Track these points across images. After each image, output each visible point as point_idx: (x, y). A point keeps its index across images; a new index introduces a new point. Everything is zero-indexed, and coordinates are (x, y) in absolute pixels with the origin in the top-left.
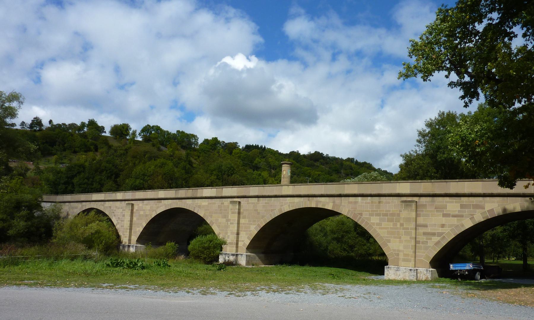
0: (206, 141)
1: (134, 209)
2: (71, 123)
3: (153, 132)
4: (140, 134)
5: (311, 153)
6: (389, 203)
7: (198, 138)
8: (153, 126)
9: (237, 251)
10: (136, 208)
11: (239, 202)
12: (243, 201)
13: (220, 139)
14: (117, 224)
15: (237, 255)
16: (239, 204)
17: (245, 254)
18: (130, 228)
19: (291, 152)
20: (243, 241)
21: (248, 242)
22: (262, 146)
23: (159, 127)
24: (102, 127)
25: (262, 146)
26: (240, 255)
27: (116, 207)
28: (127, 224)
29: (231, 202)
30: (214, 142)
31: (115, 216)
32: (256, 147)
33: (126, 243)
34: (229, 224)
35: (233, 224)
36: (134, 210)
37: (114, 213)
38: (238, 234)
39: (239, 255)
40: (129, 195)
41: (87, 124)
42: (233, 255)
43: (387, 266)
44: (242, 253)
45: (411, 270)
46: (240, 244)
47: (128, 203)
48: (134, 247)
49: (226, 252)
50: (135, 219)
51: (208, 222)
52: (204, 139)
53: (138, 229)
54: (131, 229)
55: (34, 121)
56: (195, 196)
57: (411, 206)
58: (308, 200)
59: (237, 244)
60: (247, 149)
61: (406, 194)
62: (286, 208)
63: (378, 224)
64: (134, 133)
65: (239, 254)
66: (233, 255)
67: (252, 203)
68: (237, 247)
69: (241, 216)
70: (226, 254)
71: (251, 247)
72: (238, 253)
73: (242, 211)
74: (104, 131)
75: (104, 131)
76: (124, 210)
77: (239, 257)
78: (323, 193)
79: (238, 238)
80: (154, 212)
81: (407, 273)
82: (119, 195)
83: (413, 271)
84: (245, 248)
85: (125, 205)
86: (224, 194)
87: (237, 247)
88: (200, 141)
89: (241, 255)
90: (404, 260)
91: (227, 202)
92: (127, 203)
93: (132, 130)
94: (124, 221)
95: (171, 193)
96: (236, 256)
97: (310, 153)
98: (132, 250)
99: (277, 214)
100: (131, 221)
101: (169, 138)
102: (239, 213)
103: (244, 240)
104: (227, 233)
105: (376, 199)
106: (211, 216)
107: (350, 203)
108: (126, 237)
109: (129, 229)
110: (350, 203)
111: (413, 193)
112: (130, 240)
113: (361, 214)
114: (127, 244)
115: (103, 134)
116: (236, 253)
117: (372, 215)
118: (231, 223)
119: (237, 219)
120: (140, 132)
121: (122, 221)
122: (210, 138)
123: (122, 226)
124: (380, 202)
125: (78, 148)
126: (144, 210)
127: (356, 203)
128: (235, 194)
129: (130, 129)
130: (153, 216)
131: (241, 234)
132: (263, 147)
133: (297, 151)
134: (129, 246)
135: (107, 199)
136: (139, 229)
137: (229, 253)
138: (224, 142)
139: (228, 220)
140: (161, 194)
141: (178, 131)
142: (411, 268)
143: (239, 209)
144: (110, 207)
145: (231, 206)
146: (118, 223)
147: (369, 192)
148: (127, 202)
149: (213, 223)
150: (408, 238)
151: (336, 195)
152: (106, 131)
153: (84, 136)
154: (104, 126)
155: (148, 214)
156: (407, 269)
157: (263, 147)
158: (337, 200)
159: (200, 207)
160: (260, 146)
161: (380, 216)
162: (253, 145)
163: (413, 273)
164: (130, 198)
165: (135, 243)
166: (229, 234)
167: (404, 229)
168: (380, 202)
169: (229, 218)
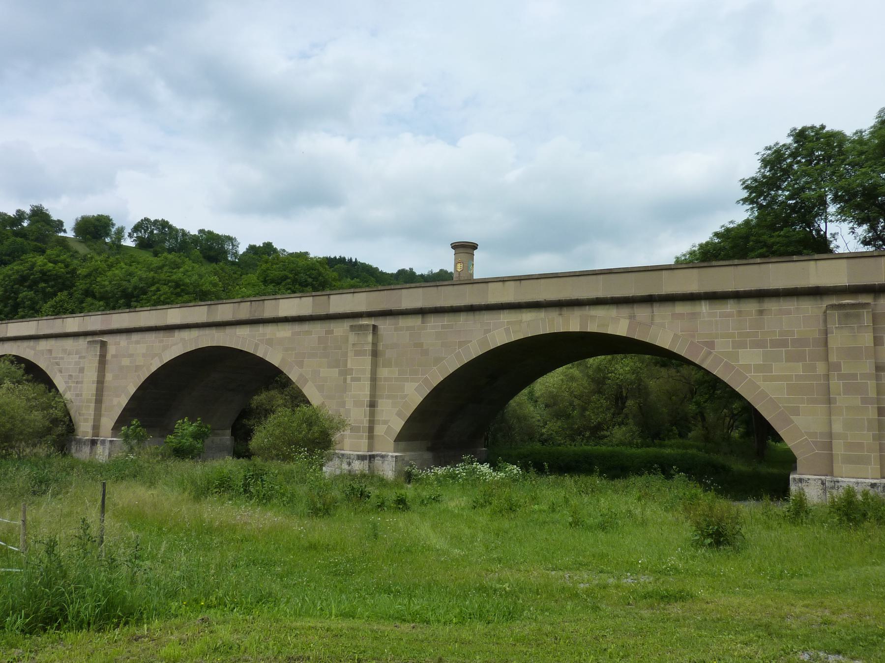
0: (252, 249)
1: (107, 354)
3: (155, 232)
4: (130, 236)
5: (433, 272)
6: (789, 312)
7: (239, 244)
8: (156, 221)
9: (371, 447)
10: (112, 350)
11: (375, 328)
12: (385, 325)
13: (277, 246)
14: (65, 391)
15: (372, 457)
16: (373, 331)
17: (390, 454)
18: (96, 399)
19: (399, 271)
20: (385, 422)
21: (398, 425)
23: (167, 222)
24: (59, 221)
26: (379, 458)
27: (64, 351)
28: (89, 389)
29: (352, 328)
31: (61, 372)
32: (342, 260)
33: (86, 433)
34: (349, 381)
35: (358, 379)
36: (109, 357)
37: (58, 364)
38: (372, 405)
39: (376, 459)
40: (95, 322)
41: (27, 214)
42: (361, 458)
44: (383, 453)
46: (379, 430)
47: (93, 341)
48: (108, 445)
49: (343, 452)
50: (109, 377)
51: (293, 377)
53: (115, 401)
54: (99, 401)
56: (257, 316)
59: (371, 429)
63: (758, 368)
64: (120, 231)
65: (377, 455)
66: (361, 458)
67: (408, 328)
68: (371, 436)
69: (381, 360)
70: (343, 455)
71: (406, 436)
72: (373, 453)
73: (380, 348)
74: (64, 228)
75: (64, 228)
76: (84, 357)
77: (378, 462)
79: (372, 414)
80: (157, 358)
82: (72, 324)
84: (391, 440)
85: (86, 345)
86: (333, 309)
87: (371, 436)
88: (242, 249)
89: (383, 457)
90: (848, 460)
91: (341, 329)
92: (91, 340)
93: (116, 227)
94: (82, 382)
95: (198, 313)
96: (370, 460)
97: (432, 272)
98: (102, 454)
100: (101, 382)
101: (184, 242)
102: (375, 354)
103: (389, 420)
104: (343, 404)
105: (751, 307)
106: (301, 364)
108: (86, 420)
109: (94, 401)
111: (857, 284)
112: (96, 427)
113: (711, 345)
114: (89, 437)
115: (62, 234)
116: (370, 453)
117: (742, 345)
118: (353, 380)
119: (369, 368)
120: (130, 231)
121: (78, 382)
122: (259, 243)
123: (77, 395)
125: (9, 255)
126: (131, 356)
128: (363, 308)
129: (113, 225)
130: (154, 369)
131: (90, 426)
132: (354, 260)
133: (410, 269)
134: (93, 443)
135: (41, 333)
136: (118, 402)
137: (351, 453)
139: (345, 372)
140: (174, 315)
141: (201, 231)
143: (375, 344)
144: (50, 351)
145: (352, 338)
146: (69, 388)
147: (730, 288)
148: (89, 339)
149: (306, 381)
150: (856, 401)
152: (67, 230)
153: (22, 234)
154: (62, 220)
155: (142, 364)
156: (862, 483)
157: (354, 260)
158: (642, 313)
159: (270, 342)
160: (348, 260)
162: (335, 257)
165: (110, 435)
166: (349, 405)
169: (349, 366)
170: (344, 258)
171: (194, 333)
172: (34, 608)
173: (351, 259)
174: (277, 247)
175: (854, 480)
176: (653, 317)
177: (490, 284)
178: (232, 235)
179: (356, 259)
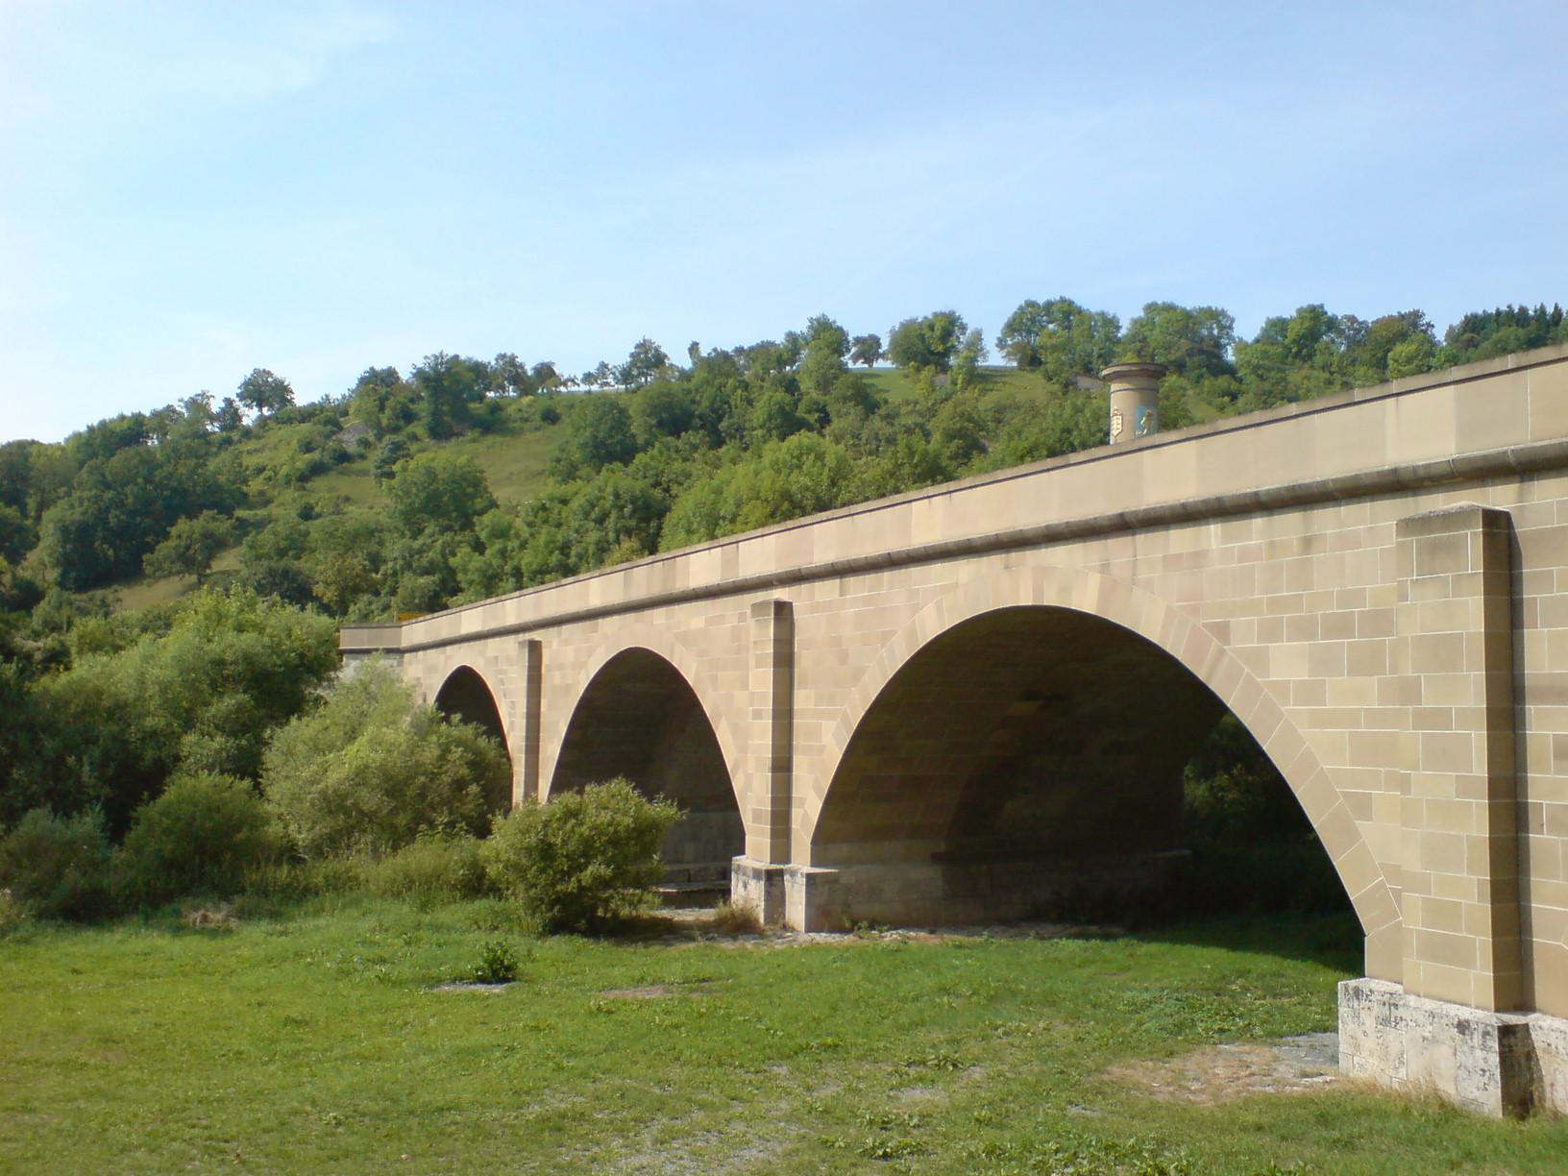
2: (759, 341)
7: (1233, 321)
8: (1049, 304)
13: (1335, 309)
22: (1542, 307)
25: (1542, 307)
30: (1307, 324)
43: (1353, 983)
45: (1463, 1027)
52: (1265, 320)
55: (639, 354)
57: (1455, 548)
58: (1007, 567)
60: (1473, 331)
61: (1434, 471)
62: (933, 625)
63: (1311, 692)
64: (976, 345)
78: (1054, 515)
81: (1445, 1050)
83: (1477, 1039)
99: (898, 654)
107: (1171, 562)
110: (1171, 562)
113: (1222, 631)
117: (1270, 632)
124: (1308, 543)
127: (1198, 558)
129: (963, 328)
132: (1550, 310)
138: (1352, 319)
142: (1465, 1013)
146: (757, 715)
151: (1105, 523)
157: (1550, 310)
159: (685, 638)
160: (1535, 312)
161: (1312, 636)
163: (1478, 1053)
164: (530, 617)
167: (1424, 719)
168: (1308, 543)
170: (1523, 310)
171: (964, 570)
172: (1260, 1088)
173: (1542, 307)
174: (1336, 313)
175: (1429, 1004)
176: (1134, 565)
177: (914, 503)
178: (1216, 304)
179: (1556, 307)
